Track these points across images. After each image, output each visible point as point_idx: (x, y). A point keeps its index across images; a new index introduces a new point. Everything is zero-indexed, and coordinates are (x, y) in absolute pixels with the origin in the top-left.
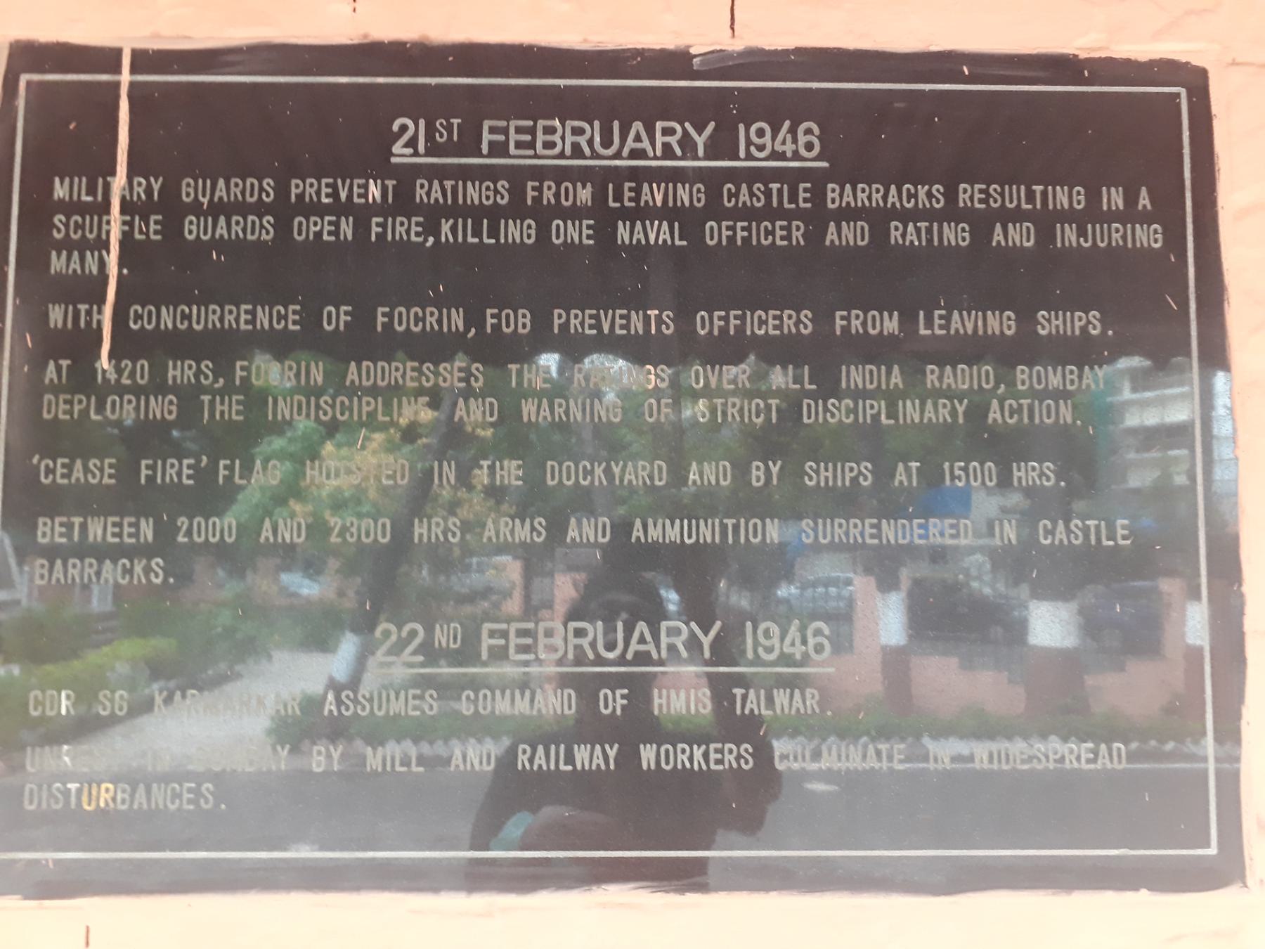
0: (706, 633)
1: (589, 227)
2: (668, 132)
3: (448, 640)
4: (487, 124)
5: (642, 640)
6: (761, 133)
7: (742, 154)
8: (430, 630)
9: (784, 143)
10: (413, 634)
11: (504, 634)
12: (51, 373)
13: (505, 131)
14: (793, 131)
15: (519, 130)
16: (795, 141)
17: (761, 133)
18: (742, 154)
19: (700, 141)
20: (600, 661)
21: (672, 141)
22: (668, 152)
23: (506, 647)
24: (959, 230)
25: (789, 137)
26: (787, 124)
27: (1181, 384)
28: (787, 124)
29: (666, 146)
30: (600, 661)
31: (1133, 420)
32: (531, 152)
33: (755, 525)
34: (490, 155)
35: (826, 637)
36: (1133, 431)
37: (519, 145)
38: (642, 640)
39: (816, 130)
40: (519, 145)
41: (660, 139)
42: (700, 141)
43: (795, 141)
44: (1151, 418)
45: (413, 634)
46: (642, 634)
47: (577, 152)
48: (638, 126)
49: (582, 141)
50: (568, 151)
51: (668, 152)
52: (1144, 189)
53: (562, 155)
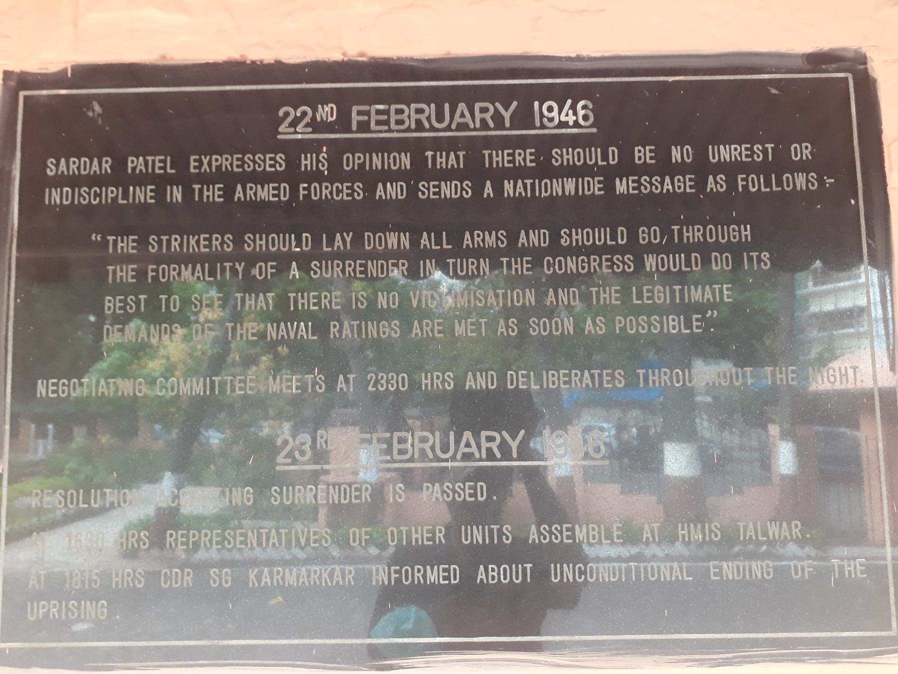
0: (506, 109)
1: (219, 189)
2: (490, 439)
3: (340, 496)
4: (355, 109)
5: (468, 445)
6: (550, 109)
7: (538, 124)
8: (315, 110)
9: (567, 115)
10: (304, 114)
11: (368, 113)
12: (63, 167)
13: (368, 113)
14: (573, 107)
15: (378, 112)
16: (575, 114)
17: (550, 109)
18: (538, 124)
19: (507, 115)
20: (433, 129)
21: (494, 446)
22: (491, 456)
23: (369, 122)
24: (245, 493)
25: (571, 112)
26: (569, 102)
27: (849, 279)
28: (569, 102)
29: (483, 121)
30: (433, 129)
31: (814, 308)
32: (386, 128)
33: (546, 184)
34: (357, 132)
35: (590, 110)
36: (815, 315)
37: (378, 123)
38: (468, 445)
39: (591, 106)
40: (378, 123)
41: (485, 445)
42: (507, 115)
43: (575, 114)
44: (829, 306)
45: (304, 114)
46: (462, 112)
47: (420, 126)
48: (462, 106)
49: (423, 118)
50: (413, 126)
51: (484, 125)
52: (488, 183)
53: (408, 130)
